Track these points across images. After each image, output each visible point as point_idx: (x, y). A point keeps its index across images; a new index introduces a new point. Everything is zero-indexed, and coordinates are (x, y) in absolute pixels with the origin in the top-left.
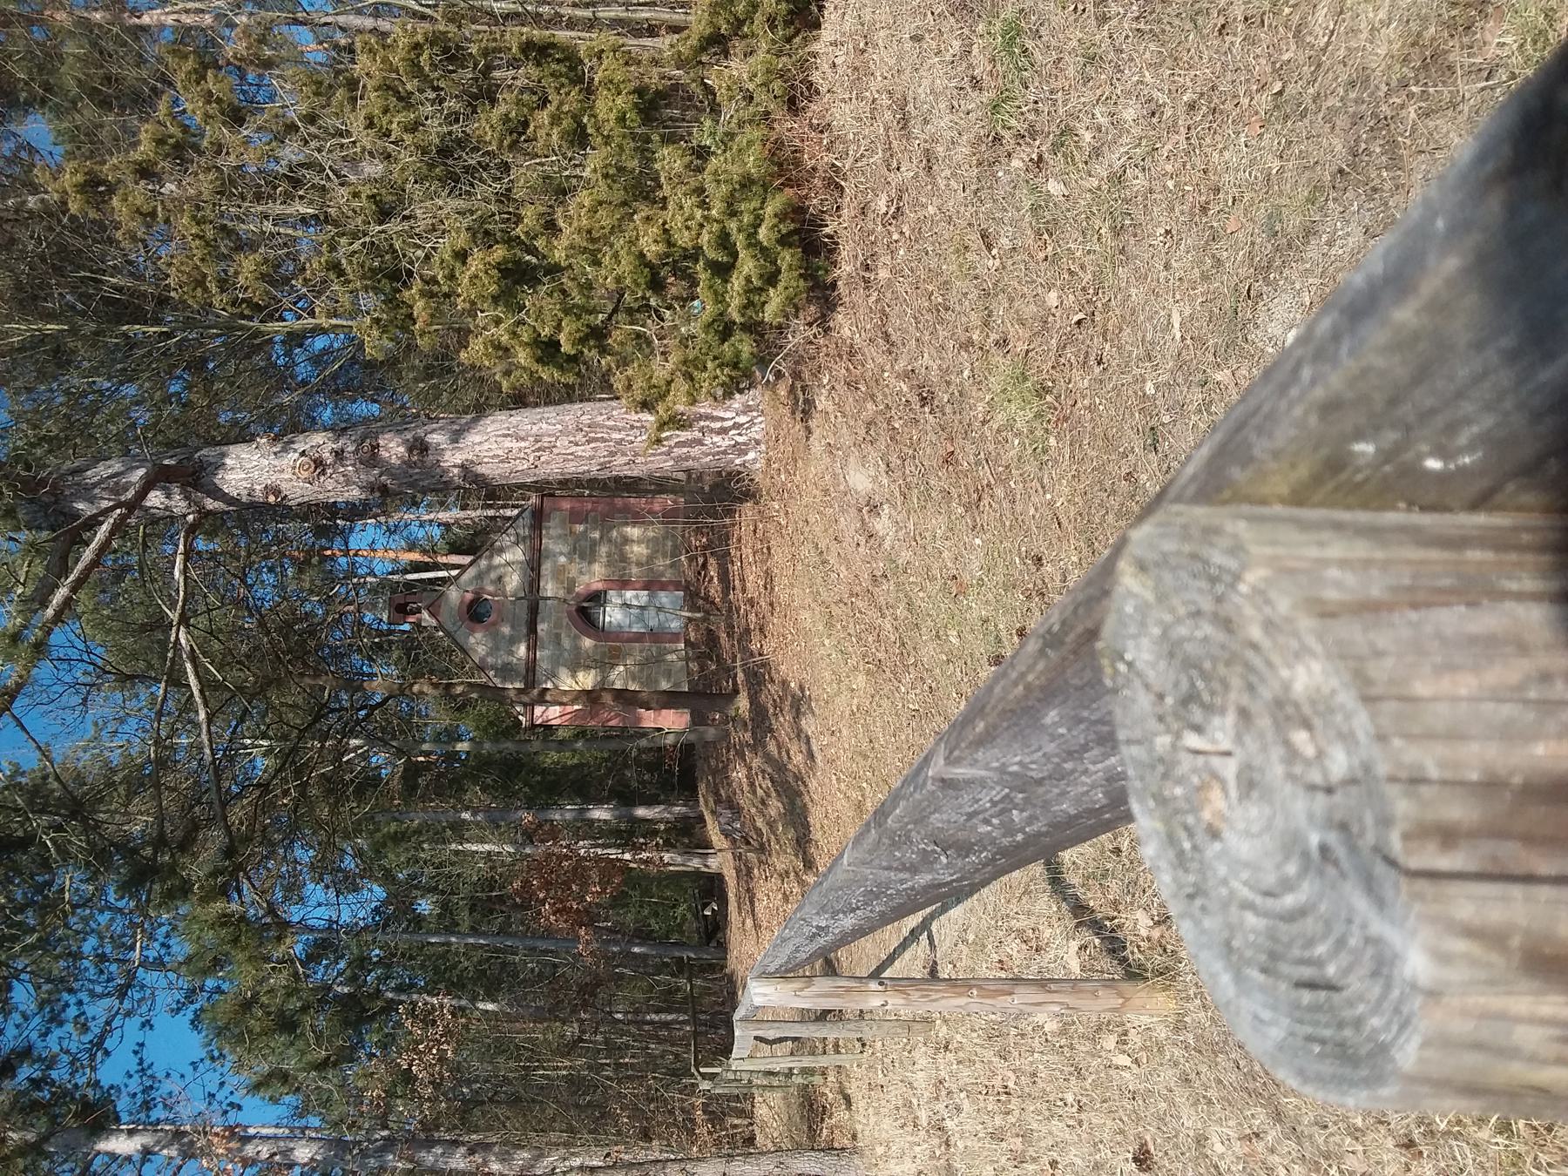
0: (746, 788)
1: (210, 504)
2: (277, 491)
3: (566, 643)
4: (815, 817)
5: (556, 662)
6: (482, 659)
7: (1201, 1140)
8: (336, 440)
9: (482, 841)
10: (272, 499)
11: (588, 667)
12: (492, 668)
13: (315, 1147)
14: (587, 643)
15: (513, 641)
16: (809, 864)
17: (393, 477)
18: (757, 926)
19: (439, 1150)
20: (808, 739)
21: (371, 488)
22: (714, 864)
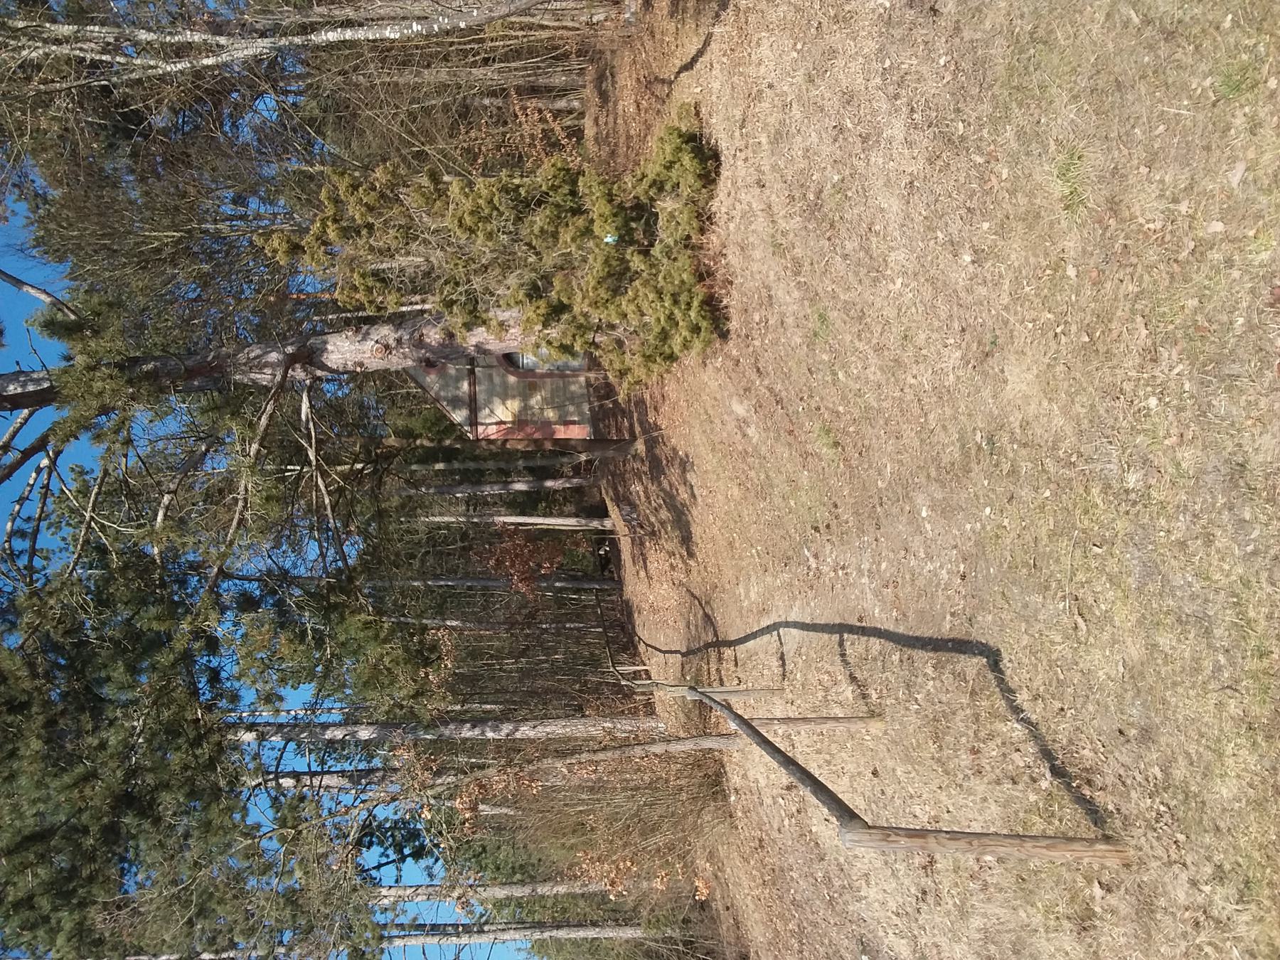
0: (643, 499)
1: (319, 373)
2: (361, 364)
3: (497, 380)
4: (696, 530)
5: (491, 393)
6: (437, 393)
7: (894, 770)
8: (397, 331)
9: (441, 514)
10: (358, 369)
11: (514, 397)
12: (445, 399)
13: (371, 729)
14: (512, 379)
15: (458, 379)
16: (691, 555)
17: (433, 353)
18: (649, 577)
19: (452, 726)
20: (692, 487)
21: (420, 360)
22: (608, 524)
